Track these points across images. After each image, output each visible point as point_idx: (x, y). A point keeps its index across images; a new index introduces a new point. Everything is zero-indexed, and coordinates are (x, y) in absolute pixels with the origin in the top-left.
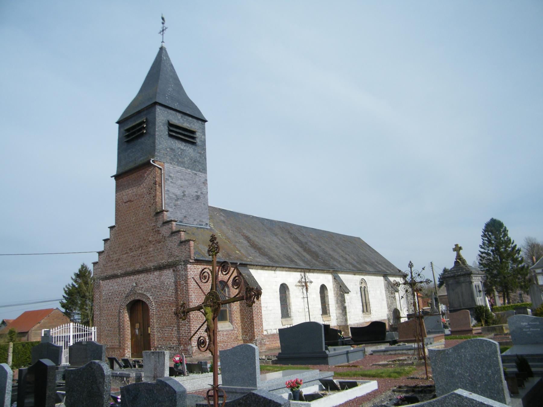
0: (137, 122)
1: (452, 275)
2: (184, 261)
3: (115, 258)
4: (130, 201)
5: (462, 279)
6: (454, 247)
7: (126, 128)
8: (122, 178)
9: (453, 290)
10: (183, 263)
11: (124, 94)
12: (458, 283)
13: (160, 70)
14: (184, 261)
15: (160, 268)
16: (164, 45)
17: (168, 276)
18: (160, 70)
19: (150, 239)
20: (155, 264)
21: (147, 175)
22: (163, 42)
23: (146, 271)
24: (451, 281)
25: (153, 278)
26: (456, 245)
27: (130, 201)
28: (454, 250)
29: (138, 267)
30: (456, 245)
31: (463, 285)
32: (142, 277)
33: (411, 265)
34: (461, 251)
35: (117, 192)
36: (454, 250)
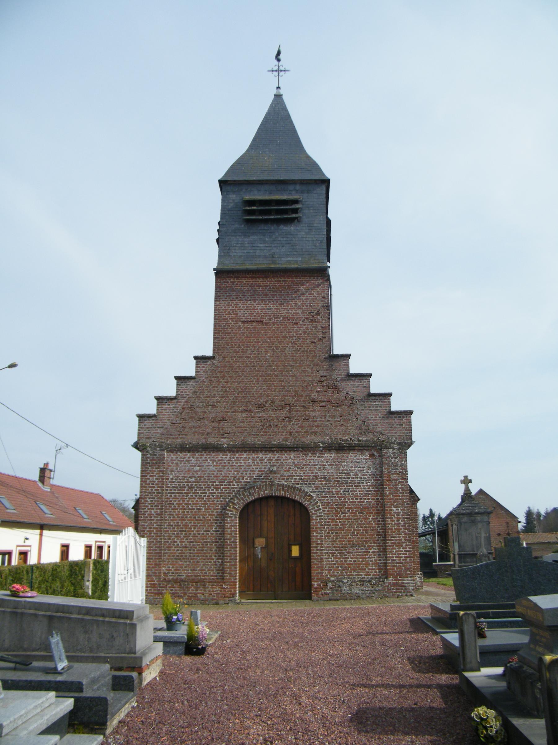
0: (285, 197)
1: (468, 511)
2: (399, 444)
3: (211, 416)
4: (260, 322)
5: (479, 518)
6: (463, 478)
7: (247, 198)
8: (237, 278)
9: (466, 530)
10: (396, 446)
11: (233, 141)
12: (474, 522)
13: (277, 127)
14: (399, 444)
15: (341, 448)
16: (281, 92)
17: (360, 465)
18: (277, 127)
19: (314, 395)
20: (326, 439)
21: (307, 290)
22: (278, 88)
23: (305, 448)
24: (465, 519)
25: (322, 464)
26: (466, 477)
27: (260, 322)
28: (462, 482)
29: (278, 440)
30: (466, 477)
31: (480, 525)
32: (289, 458)
33: (136, 495)
34: (470, 485)
35: (217, 298)
36: (462, 482)
